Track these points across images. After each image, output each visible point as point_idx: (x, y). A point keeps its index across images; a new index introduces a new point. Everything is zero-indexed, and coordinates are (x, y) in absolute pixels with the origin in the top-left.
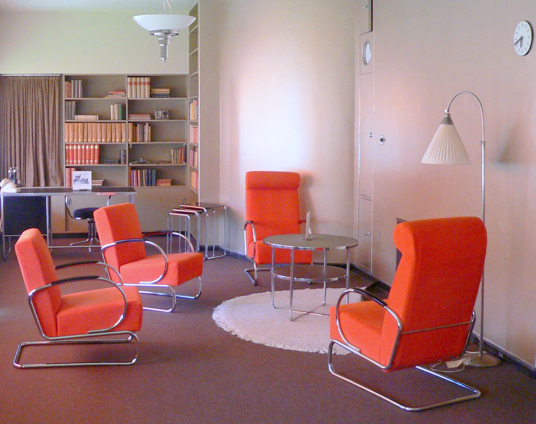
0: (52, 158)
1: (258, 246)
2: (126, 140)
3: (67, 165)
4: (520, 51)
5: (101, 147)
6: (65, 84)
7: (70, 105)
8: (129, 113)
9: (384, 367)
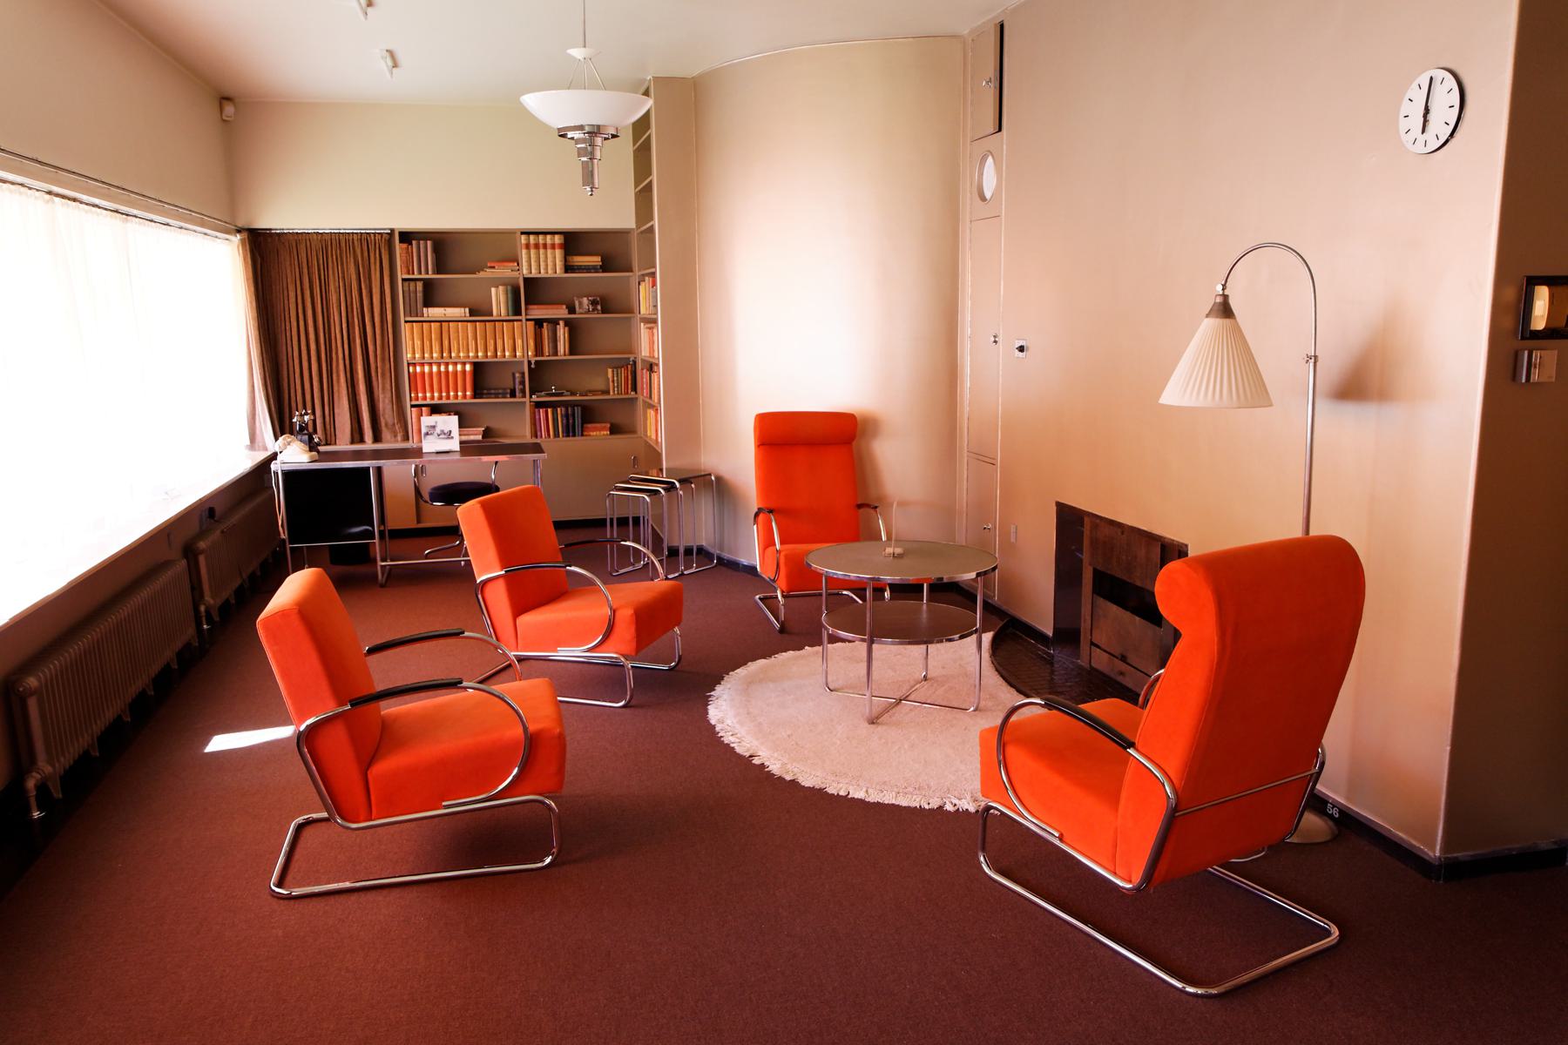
1: (786, 556)
2: (523, 352)
3: (414, 403)
4: (1420, 142)
5: (477, 366)
6: (401, 248)
8: (527, 304)
9: (1129, 886)
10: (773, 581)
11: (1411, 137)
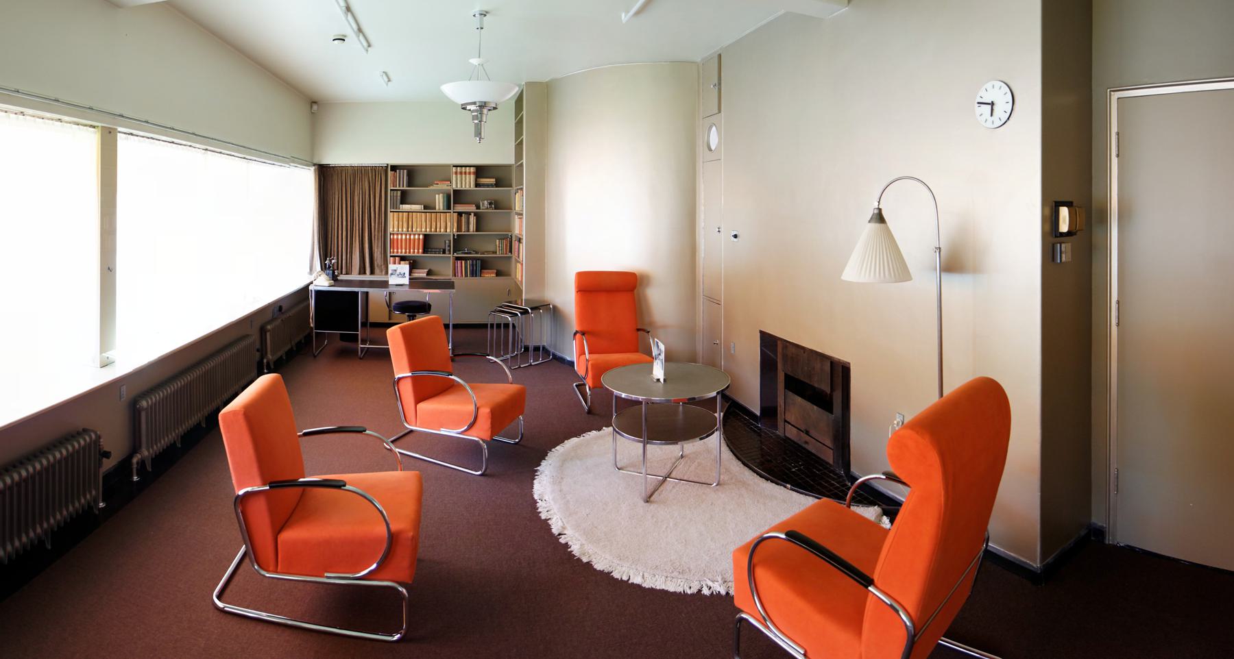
0: (377, 246)
1: (592, 365)
3: (392, 254)
5: (426, 237)
7: (395, 195)
10: (584, 378)
11: (983, 118)
